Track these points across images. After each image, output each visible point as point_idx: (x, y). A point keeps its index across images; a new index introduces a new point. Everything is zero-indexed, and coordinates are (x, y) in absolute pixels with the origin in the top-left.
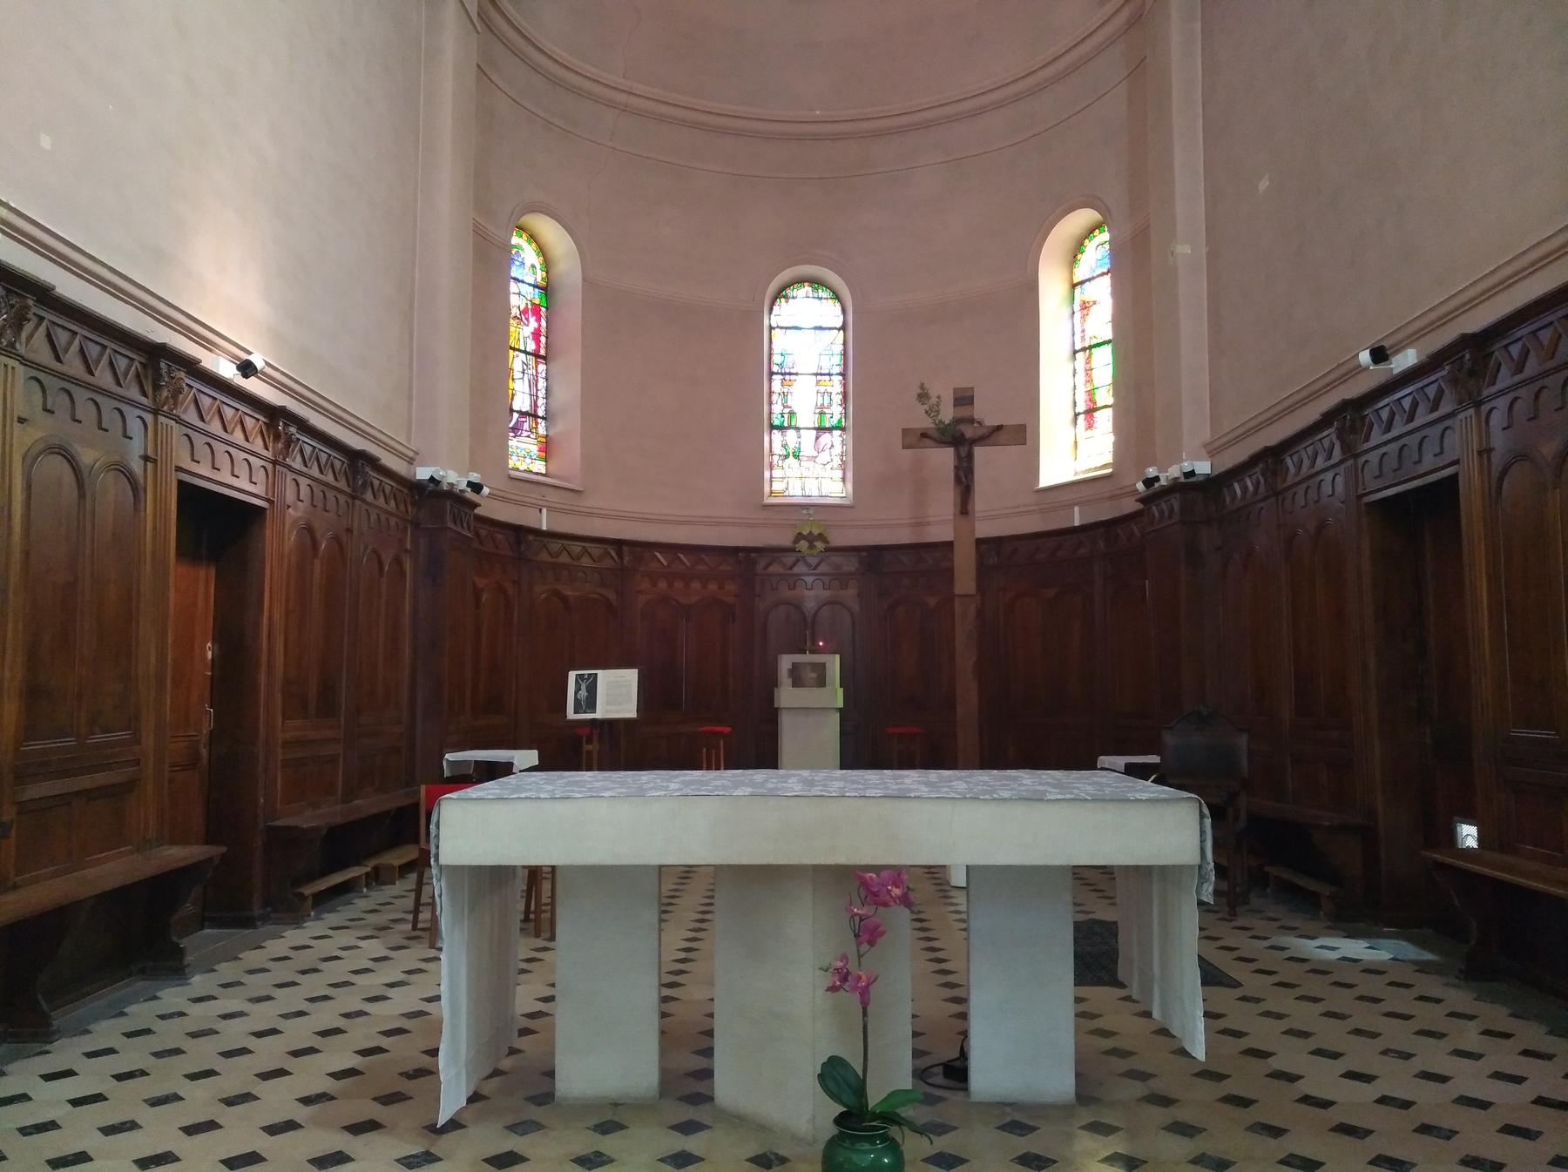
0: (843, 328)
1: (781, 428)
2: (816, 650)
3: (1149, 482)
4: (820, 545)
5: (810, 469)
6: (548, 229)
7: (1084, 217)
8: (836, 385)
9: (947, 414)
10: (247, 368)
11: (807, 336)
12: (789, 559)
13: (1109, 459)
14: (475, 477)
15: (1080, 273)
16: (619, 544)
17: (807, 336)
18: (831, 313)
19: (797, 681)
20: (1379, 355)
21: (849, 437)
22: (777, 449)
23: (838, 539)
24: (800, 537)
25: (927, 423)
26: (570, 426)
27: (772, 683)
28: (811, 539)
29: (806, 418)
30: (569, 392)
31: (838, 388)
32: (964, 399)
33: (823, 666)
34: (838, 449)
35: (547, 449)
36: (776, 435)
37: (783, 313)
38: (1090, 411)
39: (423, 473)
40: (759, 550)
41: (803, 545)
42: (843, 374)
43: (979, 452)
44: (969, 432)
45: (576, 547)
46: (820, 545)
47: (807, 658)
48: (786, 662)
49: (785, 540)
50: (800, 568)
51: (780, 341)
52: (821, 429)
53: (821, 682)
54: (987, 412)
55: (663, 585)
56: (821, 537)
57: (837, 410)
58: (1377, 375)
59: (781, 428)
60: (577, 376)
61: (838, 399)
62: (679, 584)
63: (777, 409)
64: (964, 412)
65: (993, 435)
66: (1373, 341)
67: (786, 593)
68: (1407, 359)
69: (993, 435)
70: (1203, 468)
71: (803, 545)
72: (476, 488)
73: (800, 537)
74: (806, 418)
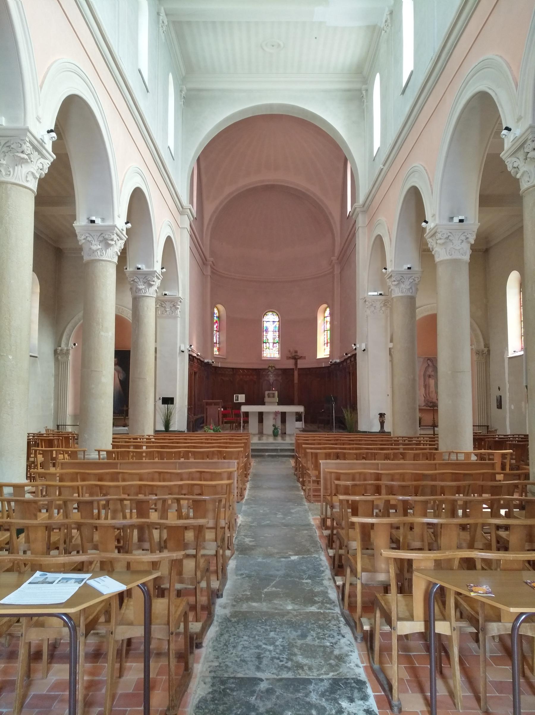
0: (279, 321)
1: (266, 343)
2: (272, 390)
3: (331, 362)
4: (274, 368)
5: (271, 351)
6: (220, 306)
7: (325, 306)
8: (277, 334)
9: (293, 355)
10: (198, 355)
11: (271, 322)
12: (267, 371)
13: (329, 353)
14: (213, 361)
15: (326, 316)
16: (233, 369)
17: (271, 322)
18: (276, 319)
19: (269, 397)
20: (346, 354)
21: (280, 345)
22: (265, 347)
23: (277, 367)
24: (269, 366)
25: (290, 356)
26: (224, 345)
27: (264, 397)
28: (272, 367)
29: (271, 340)
30: (224, 338)
31: (277, 334)
32: (296, 352)
33: (274, 394)
34: (277, 347)
35: (219, 350)
36: (265, 344)
37: (266, 318)
38: (327, 343)
39: (206, 361)
40: (260, 369)
41: (270, 368)
42: (279, 331)
43: (298, 360)
44: (297, 357)
45: (229, 370)
46: (274, 368)
47: (271, 392)
48: (267, 393)
49: (266, 367)
50: (270, 373)
51: (265, 324)
52: (274, 343)
53: (274, 397)
54: (300, 354)
55: (241, 377)
56: (274, 367)
57: (277, 339)
58: (346, 357)
59: (266, 343)
60: (225, 335)
61: (277, 336)
62: (245, 377)
63: (265, 338)
64: (296, 354)
65: (301, 358)
66: (346, 352)
67: (266, 378)
68: (349, 355)
69: (301, 358)
70: (338, 361)
71: (270, 368)
72: (213, 362)
73: (269, 366)
74: (271, 340)
